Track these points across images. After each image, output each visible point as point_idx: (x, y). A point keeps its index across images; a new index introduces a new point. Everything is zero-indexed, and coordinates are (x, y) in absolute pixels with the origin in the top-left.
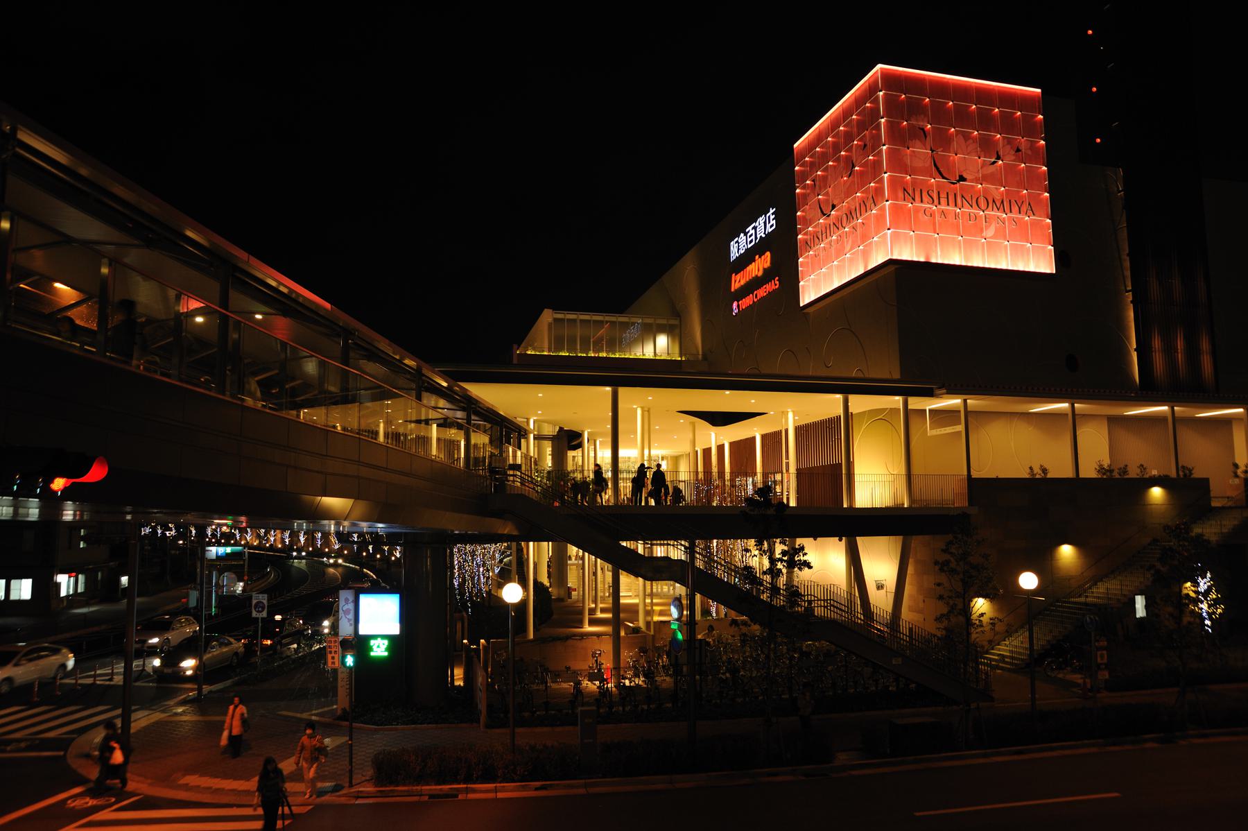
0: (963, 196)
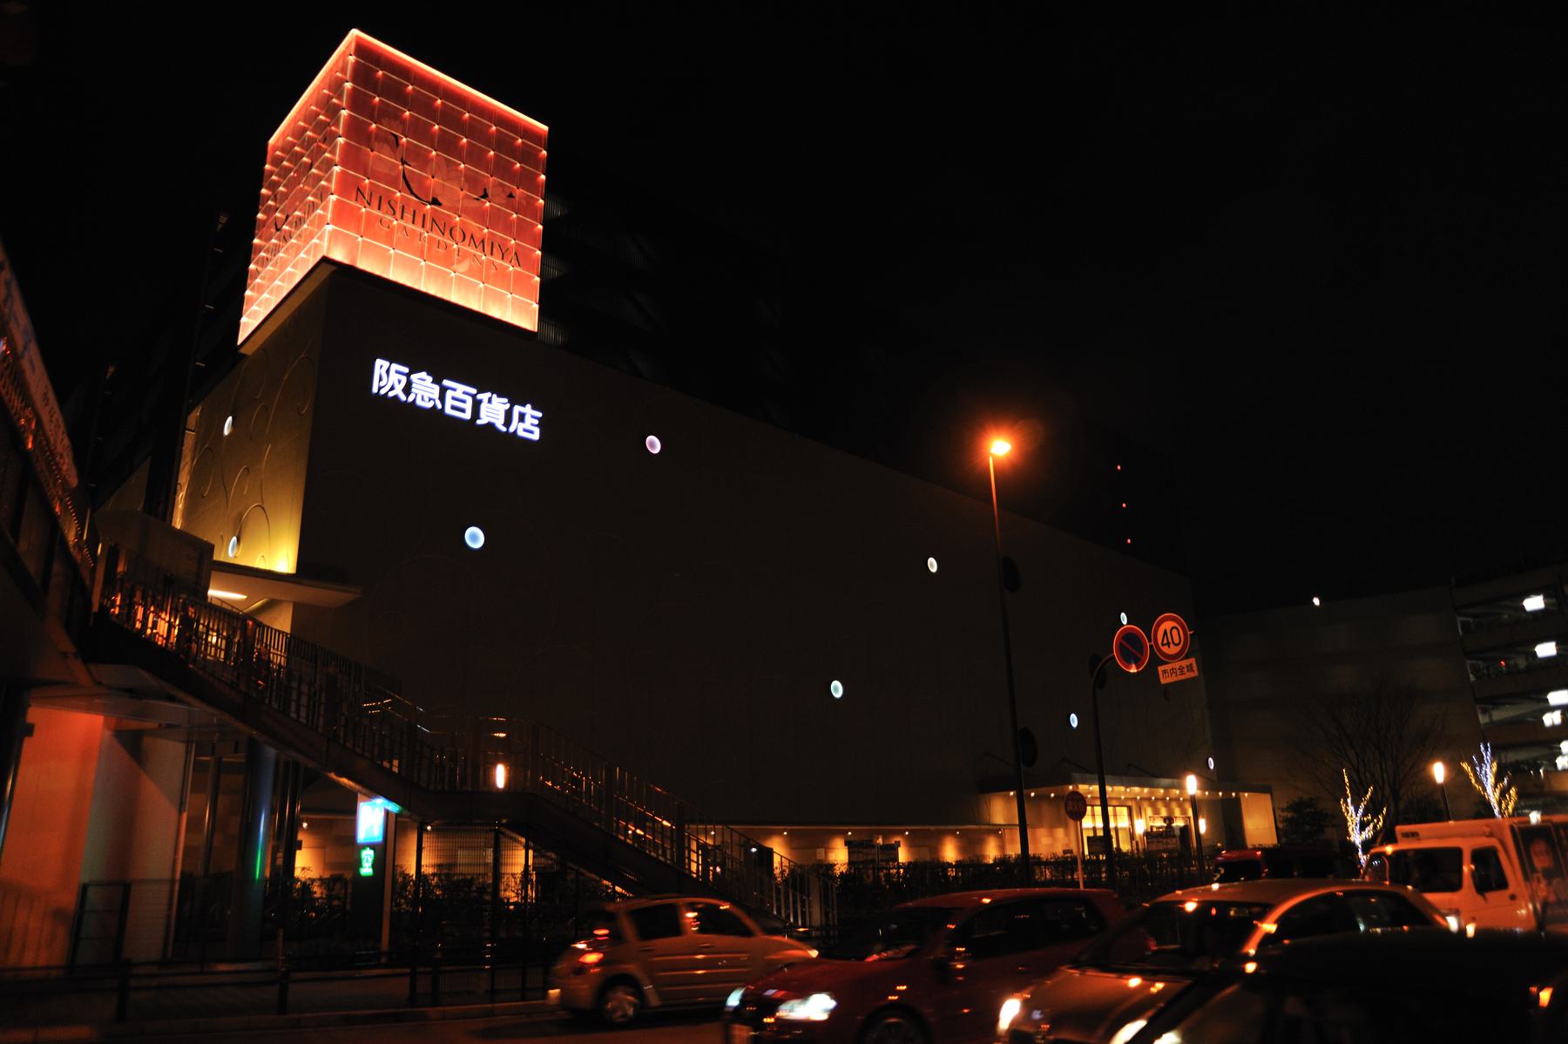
0: (433, 220)
